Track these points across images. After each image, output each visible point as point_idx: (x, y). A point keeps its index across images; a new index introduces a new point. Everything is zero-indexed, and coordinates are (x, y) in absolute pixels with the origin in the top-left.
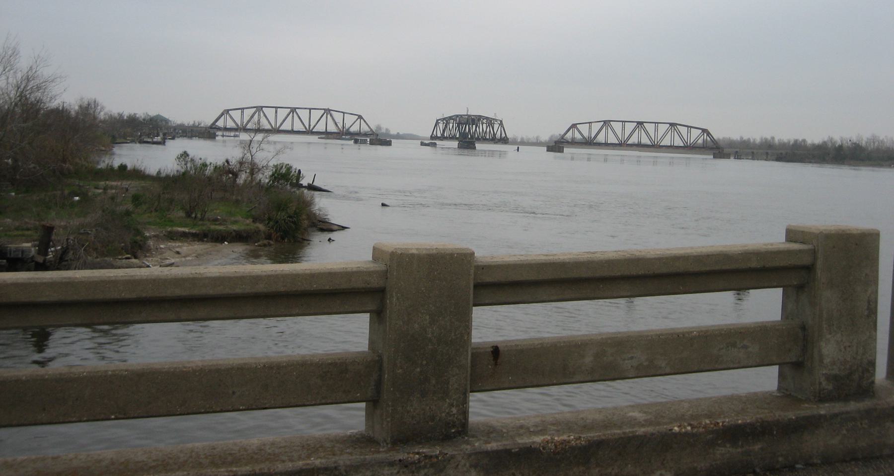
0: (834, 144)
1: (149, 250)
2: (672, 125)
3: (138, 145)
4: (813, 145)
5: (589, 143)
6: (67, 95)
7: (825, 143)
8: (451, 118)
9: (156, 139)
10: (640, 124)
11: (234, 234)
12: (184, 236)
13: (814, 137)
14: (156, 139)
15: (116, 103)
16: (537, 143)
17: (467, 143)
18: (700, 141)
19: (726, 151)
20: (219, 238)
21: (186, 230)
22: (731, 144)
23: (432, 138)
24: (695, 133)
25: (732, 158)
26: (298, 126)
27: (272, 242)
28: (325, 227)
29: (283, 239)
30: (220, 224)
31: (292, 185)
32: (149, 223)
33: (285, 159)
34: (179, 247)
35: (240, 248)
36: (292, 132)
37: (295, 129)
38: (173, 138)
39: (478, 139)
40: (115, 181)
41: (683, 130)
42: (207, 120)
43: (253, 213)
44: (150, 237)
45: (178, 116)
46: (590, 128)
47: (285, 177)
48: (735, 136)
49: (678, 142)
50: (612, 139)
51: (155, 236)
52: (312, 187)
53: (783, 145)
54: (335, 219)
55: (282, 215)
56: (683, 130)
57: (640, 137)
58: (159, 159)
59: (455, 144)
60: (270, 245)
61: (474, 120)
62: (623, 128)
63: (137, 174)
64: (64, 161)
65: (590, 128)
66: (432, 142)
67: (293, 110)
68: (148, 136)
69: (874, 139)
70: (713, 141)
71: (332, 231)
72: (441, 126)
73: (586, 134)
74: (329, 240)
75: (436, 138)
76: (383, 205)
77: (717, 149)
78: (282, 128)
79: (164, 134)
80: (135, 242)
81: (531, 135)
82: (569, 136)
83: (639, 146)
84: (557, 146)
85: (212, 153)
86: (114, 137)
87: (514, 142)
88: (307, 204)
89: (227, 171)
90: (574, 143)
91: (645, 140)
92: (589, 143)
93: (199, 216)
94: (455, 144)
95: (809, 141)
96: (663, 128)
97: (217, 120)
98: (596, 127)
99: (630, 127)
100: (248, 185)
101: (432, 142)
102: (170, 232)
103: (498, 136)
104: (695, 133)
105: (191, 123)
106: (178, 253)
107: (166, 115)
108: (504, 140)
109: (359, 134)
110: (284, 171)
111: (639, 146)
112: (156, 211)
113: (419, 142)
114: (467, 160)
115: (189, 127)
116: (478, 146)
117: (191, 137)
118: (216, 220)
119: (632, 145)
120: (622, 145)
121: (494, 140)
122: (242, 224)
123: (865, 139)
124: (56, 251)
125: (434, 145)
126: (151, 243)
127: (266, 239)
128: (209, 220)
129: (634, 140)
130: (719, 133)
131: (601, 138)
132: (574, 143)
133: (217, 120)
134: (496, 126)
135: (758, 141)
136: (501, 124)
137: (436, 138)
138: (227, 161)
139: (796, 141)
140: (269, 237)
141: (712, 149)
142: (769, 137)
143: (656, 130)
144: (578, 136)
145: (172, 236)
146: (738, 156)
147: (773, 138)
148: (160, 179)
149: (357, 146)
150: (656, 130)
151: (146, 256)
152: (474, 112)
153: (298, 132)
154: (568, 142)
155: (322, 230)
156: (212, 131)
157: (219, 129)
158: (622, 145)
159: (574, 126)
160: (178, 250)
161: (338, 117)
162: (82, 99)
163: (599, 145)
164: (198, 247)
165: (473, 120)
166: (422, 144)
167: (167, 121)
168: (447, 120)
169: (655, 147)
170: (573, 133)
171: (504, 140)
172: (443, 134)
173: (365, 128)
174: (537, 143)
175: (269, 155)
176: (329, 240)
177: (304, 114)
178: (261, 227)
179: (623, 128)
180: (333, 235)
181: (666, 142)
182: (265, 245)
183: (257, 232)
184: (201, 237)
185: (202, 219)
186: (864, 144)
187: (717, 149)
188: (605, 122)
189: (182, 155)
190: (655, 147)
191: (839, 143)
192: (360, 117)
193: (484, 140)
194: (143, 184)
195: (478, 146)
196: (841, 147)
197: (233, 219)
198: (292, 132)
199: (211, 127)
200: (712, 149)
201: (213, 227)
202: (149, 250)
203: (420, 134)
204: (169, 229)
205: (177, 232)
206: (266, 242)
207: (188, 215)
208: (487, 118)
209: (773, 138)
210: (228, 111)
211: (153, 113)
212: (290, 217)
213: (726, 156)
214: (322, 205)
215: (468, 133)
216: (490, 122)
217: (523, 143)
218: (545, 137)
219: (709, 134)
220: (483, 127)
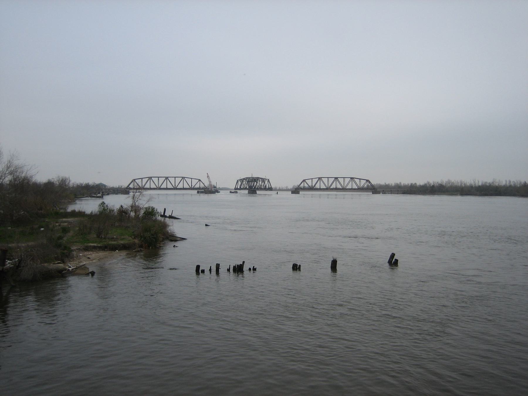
0: (430, 185)
1: (72, 258)
2: (352, 178)
3: (90, 198)
4: (420, 186)
5: (312, 188)
6: (41, 176)
7: (426, 184)
8: (244, 179)
9: (98, 195)
10: (336, 178)
11: (121, 246)
12: (95, 248)
13: (420, 182)
14: (98, 195)
15: (77, 178)
16: (287, 190)
17: (252, 191)
18: (366, 186)
19: (378, 190)
20: (113, 248)
21: (95, 245)
22: (381, 187)
23: (235, 189)
24: (363, 182)
25: (381, 194)
26: (169, 186)
27: (142, 249)
28: (173, 238)
29: (149, 247)
30: (115, 241)
31: (161, 216)
32: (76, 242)
33: (152, 204)
34: (91, 254)
35: (124, 253)
36: (167, 189)
37: (152, 187)
38: (108, 194)
39: (258, 189)
40: (69, 218)
41: (357, 181)
42: (125, 184)
43: (135, 233)
44: (75, 250)
45: (111, 183)
46: (312, 181)
47: (150, 213)
48: (382, 183)
49: (355, 187)
50: (323, 187)
51: (77, 249)
52: (171, 217)
53: (405, 187)
54: (179, 234)
55: (147, 234)
56: (357, 181)
57: (336, 185)
58: (89, 206)
59: (247, 192)
60: (141, 251)
61: (256, 180)
62: (328, 180)
63: (81, 214)
64: (41, 209)
65: (312, 181)
66: (236, 191)
67: (167, 178)
68: (95, 194)
69: (449, 182)
70: (372, 185)
71: (176, 241)
72: (239, 183)
73: (310, 185)
74: (174, 246)
75: (237, 189)
76: (206, 225)
77: (374, 189)
78: (162, 187)
79: (103, 193)
80: (64, 253)
81: (284, 186)
82: (302, 185)
83: (336, 189)
84: (296, 191)
85: (115, 202)
86: (75, 195)
87: (276, 190)
88: (164, 226)
89: (122, 212)
90: (304, 189)
91: (339, 186)
92: (312, 188)
93: (103, 236)
94: (247, 192)
95: (418, 184)
96: (347, 180)
97: (129, 185)
98: (315, 181)
99: (331, 180)
100: (137, 217)
101: (236, 191)
102: (87, 247)
103: (267, 187)
104: (363, 182)
105: (117, 186)
106: (89, 258)
107: (104, 183)
108: (270, 189)
109: (199, 188)
110: (150, 210)
111: (336, 189)
112: (82, 234)
113: (229, 191)
114: (252, 199)
115: (116, 188)
116: (258, 192)
117: (117, 194)
118: (113, 238)
119: (332, 189)
120: (328, 189)
121: (265, 189)
122: (127, 240)
123: (445, 182)
124: (15, 262)
125: (237, 192)
126: (74, 253)
127: (139, 247)
128: (109, 239)
129: (333, 186)
130: (375, 181)
131: (317, 186)
132: (304, 189)
133: (129, 185)
134: (266, 182)
135: (393, 185)
136: (269, 181)
137: (237, 189)
138: (122, 206)
139: (412, 184)
140: (141, 246)
141: (371, 189)
142: (399, 183)
143: (344, 181)
144: (306, 185)
145: (87, 249)
146: (384, 192)
147: (400, 183)
148: (91, 216)
149: (198, 194)
150: (344, 181)
151: (70, 261)
152: (255, 176)
153: (154, 189)
154: (301, 189)
155: (172, 241)
156: (128, 190)
157: (131, 189)
158: (328, 189)
159: (304, 181)
160: (88, 256)
161: (189, 181)
162: (59, 177)
163: (317, 189)
164: (101, 254)
165: (255, 180)
166: (231, 192)
167: (105, 186)
168: (242, 180)
169: (344, 189)
170: (304, 184)
171: (270, 189)
172: (240, 187)
173: (202, 186)
174: (287, 190)
175: (144, 203)
176: (174, 246)
177: (172, 180)
178: (136, 241)
179: (328, 180)
180: (177, 244)
181: (349, 187)
182: (138, 251)
183: (134, 244)
184: (104, 248)
185: (105, 238)
186: (444, 184)
187: (374, 189)
188: (335, 178)
189: (101, 204)
190: (344, 189)
191: (432, 184)
192: (200, 180)
193: (261, 189)
194: (82, 219)
195: (258, 192)
196: (433, 186)
197: (122, 237)
198: (167, 189)
199: (127, 188)
200: (371, 189)
201: (110, 242)
202: (72, 258)
203: (231, 188)
204: (86, 244)
205: (91, 246)
206: (139, 249)
207: (98, 236)
208: (262, 178)
209: (400, 183)
210: (135, 180)
211: (97, 182)
212: (152, 235)
213: (378, 193)
214: (175, 228)
215: (252, 186)
216: (263, 180)
217: (280, 190)
218: (290, 187)
219: (369, 182)
220: (260, 183)
